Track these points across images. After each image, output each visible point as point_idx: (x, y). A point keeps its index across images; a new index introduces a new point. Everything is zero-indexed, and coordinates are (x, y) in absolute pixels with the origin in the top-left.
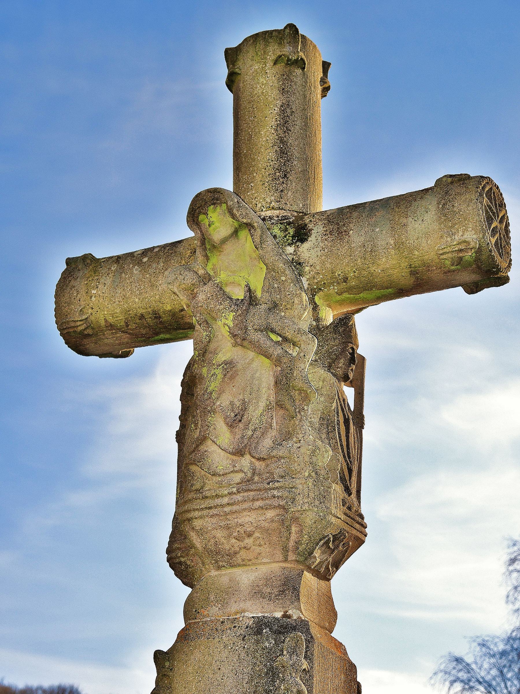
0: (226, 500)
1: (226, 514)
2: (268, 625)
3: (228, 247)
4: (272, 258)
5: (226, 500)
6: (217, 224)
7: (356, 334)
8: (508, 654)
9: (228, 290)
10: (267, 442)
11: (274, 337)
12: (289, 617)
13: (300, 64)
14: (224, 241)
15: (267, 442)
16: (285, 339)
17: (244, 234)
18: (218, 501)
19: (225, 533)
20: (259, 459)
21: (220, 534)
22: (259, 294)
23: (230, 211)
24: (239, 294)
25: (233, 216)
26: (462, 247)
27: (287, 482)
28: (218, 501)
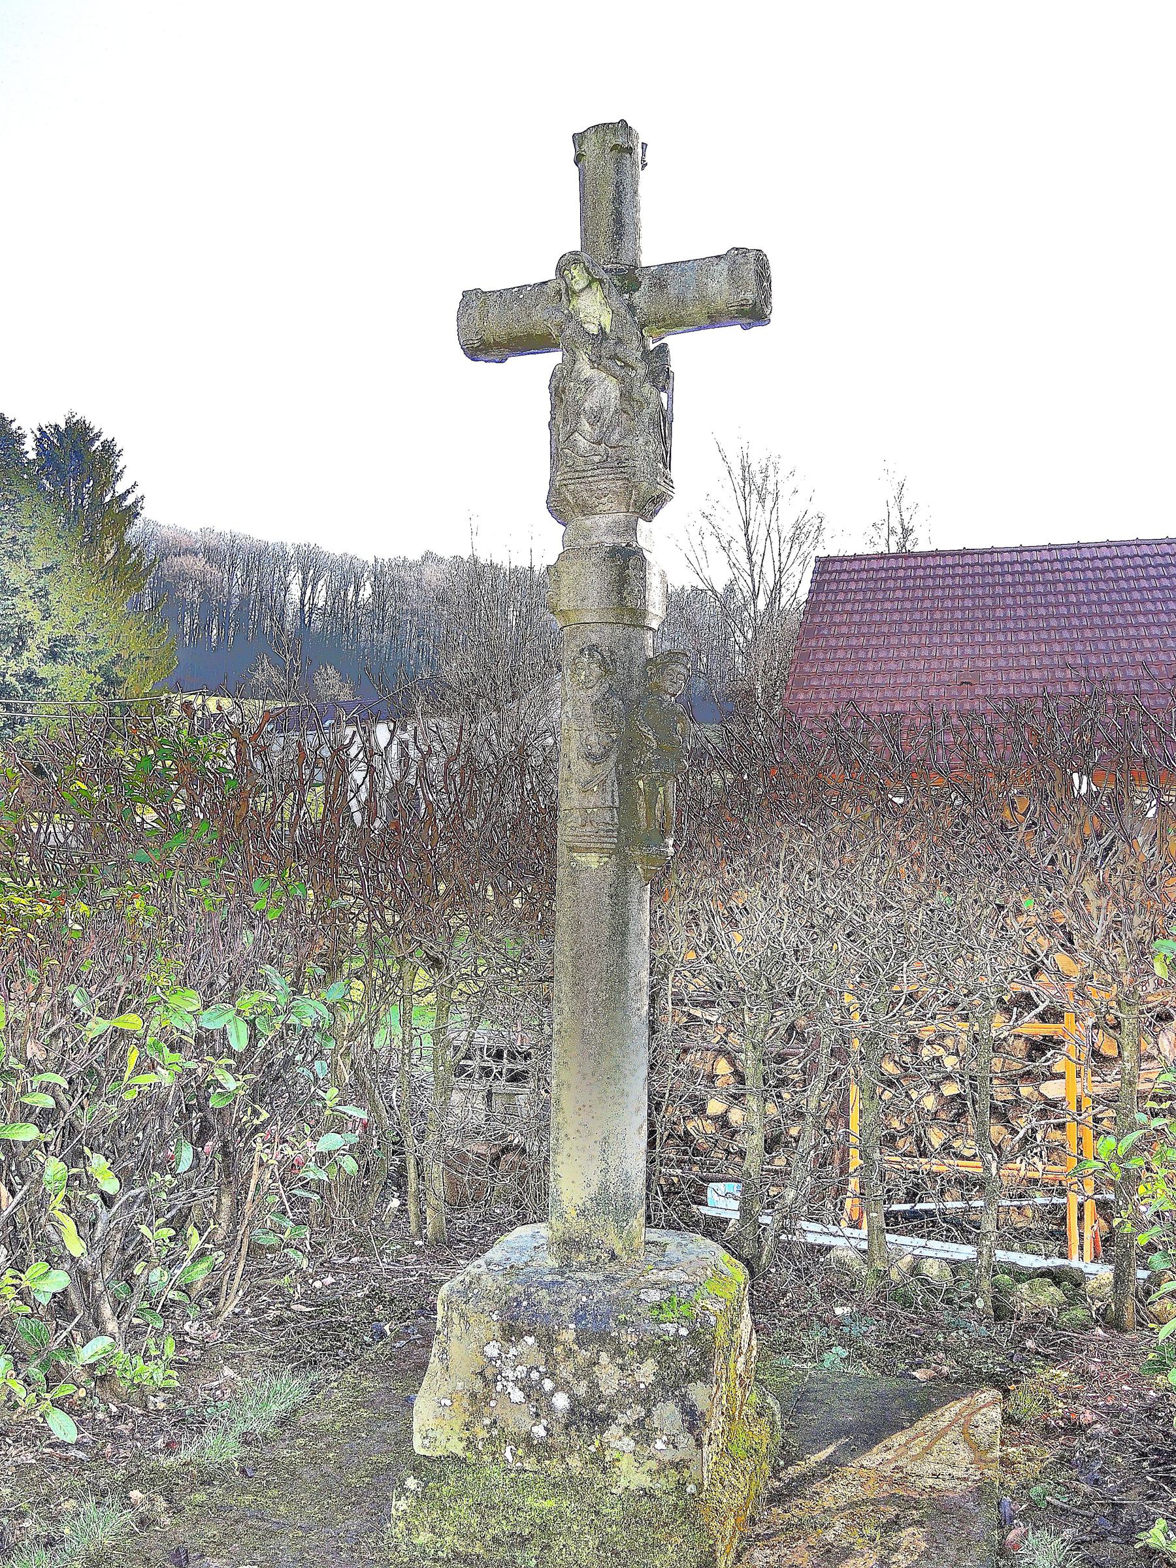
0: (590, 473)
1: (590, 482)
2: (618, 551)
3: (584, 295)
4: (616, 304)
5: (590, 473)
6: (577, 278)
7: (726, 1246)
8: (597, 750)
9: (586, 326)
10: (616, 436)
11: (619, 363)
12: (631, 546)
13: (630, 150)
14: (582, 290)
15: (616, 436)
16: (626, 365)
17: (595, 285)
18: (585, 474)
19: (589, 494)
20: (611, 447)
21: (585, 494)
22: (608, 330)
23: (587, 269)
24: (594, 330)
25: (589, 273)
26: (744, 302)
27: (631, 463)
28: (585, 474)
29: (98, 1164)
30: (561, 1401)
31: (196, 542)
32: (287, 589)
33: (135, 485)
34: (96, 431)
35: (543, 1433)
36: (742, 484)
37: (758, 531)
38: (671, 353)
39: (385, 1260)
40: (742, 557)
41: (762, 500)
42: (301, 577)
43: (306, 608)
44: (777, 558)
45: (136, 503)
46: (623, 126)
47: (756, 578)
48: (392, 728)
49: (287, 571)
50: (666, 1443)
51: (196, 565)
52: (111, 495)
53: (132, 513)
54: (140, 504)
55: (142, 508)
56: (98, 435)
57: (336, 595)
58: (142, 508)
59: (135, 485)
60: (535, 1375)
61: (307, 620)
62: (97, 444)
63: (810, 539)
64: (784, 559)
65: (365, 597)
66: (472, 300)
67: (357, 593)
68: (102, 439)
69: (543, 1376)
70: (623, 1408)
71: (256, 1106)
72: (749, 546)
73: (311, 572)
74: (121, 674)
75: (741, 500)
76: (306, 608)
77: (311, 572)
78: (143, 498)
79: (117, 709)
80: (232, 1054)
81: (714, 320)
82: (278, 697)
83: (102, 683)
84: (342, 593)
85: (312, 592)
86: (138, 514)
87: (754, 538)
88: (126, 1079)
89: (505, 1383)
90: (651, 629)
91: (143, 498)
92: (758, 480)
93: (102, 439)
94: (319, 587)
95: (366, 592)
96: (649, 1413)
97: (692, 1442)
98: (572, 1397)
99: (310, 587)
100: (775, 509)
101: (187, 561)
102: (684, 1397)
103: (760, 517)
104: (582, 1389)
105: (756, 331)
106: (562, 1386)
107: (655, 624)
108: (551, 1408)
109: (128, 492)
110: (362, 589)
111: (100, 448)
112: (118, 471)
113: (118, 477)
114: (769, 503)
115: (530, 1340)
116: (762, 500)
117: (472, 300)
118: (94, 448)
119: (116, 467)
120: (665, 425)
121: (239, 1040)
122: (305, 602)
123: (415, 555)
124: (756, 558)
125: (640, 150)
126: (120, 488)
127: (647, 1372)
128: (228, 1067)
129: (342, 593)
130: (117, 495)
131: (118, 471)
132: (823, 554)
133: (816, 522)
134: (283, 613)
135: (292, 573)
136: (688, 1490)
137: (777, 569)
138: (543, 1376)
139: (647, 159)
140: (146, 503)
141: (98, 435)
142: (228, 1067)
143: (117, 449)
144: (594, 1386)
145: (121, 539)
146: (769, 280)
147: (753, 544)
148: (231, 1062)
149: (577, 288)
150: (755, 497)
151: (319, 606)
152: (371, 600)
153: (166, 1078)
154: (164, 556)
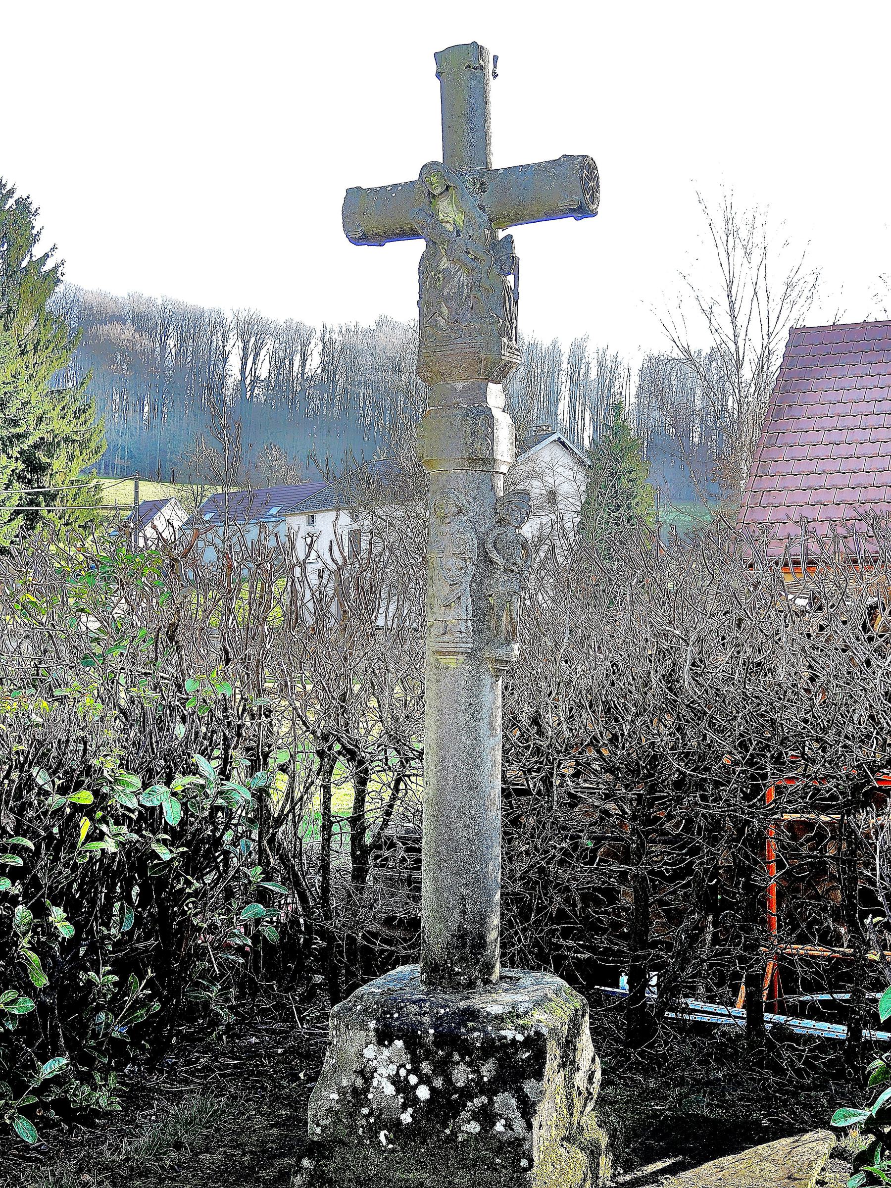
29: (57, 914)
30: (423, 1093)
31: (124, 308)
32: (225, 359)
33: (54, 248)
34: (8, 187)
35: (410, 1120)
36: (724, 238)
37: (743, 293)
38: (516, 243)
39: (305, 1026)
40: (725, 321)
41: (748, 254)
42: (241, 345)
43: (248, 381)
44: (765, 322)
45: (56, 267)
46: (477, 49)
47: (741, 343)
48: (309, 542)
49: (225, 338)
50: (505, 1126)
51: (126, 333)
52: (27, 259)
53: (53, 278)
54: (60, 269)
55: (63, 274)
56: (11, 193)
57: (280, 365)
58: (63, 274)
59: (54, 248)
60: (403, 1072)
61: (249, 394)
62: (11, 202)
63: (804, 298)
64: (772, 324)
65: (312, 367)
66: (354, 195)
67: (304, 361)
68: (16, 196)
69: (409, 1072)
70: (471, 1097)
71: (189, 877)
72: (732, 308)
73: (253, 340)
74: (44, 459)
75: (724, 256)
76: (248, 381)
77: (253, 340)
78: (63, 262)
79: (41, 498)
80: (167, 828)
81: (551, 214)
82: (217, 479)
83: (23, 470)
84: (287, 363)
85: (254, 363)
86: (59, 280)
87: (739, 298)
88: (79, 845)
89: (380, 1079)
90: (499, 473)
91: (63, 262)
92: (744, 233)
93: (16, 196)
94: (262, 357)
95: (314, 363)
96: (491, 1101)
97: (524, 1124)
98: (433, 1090)
99: (251, 357)
100: (763, 266)
101: (114, 331)
102: (521, 1089)
103: (745, 274)
104: (438, 1083)
105: (586, 221)
106: (425, 1080)
107: (504, 469)
108: (416, 1099)
109: (46, 256)
110: (310, 358)
111: (14, 207)
112: (34, 232)
113: (35, 239)
114: (756, 257)
115: (399, 1044)
116: (748, 254)
117: (354, 195)
118: (7, 207)
119: (33, 228)
120: (510, 303)
121: (173, 814)
122: (247, 374)
123: (368, 322)
124: (741, 320)
125: (491, 66)
126: (38, 251)
127: (488, 1070)
128: (164, 842)
129: (287, 363)
130: (34, 259)
131: (34, 232)
132: (817, 318)
133: (811, 279)
134: (223, 382)
135: (231, 342)
136: (522, 1164)
137: (765, 332)
138: (409, 1072)
139: (497, 70)
140: (66, 269)
141: (11, 193)
142: (164, 842)
143: (33, 208)
144: (448, 1080)
145: (41, 309)
146: (596, 179)
147: (737, 306)
148: (166, 837)
149: (436, 192)
150: (740, 252)
151: (262, 378)
152: (319, 371)
153: (110, 846)
154: (89, 323)
